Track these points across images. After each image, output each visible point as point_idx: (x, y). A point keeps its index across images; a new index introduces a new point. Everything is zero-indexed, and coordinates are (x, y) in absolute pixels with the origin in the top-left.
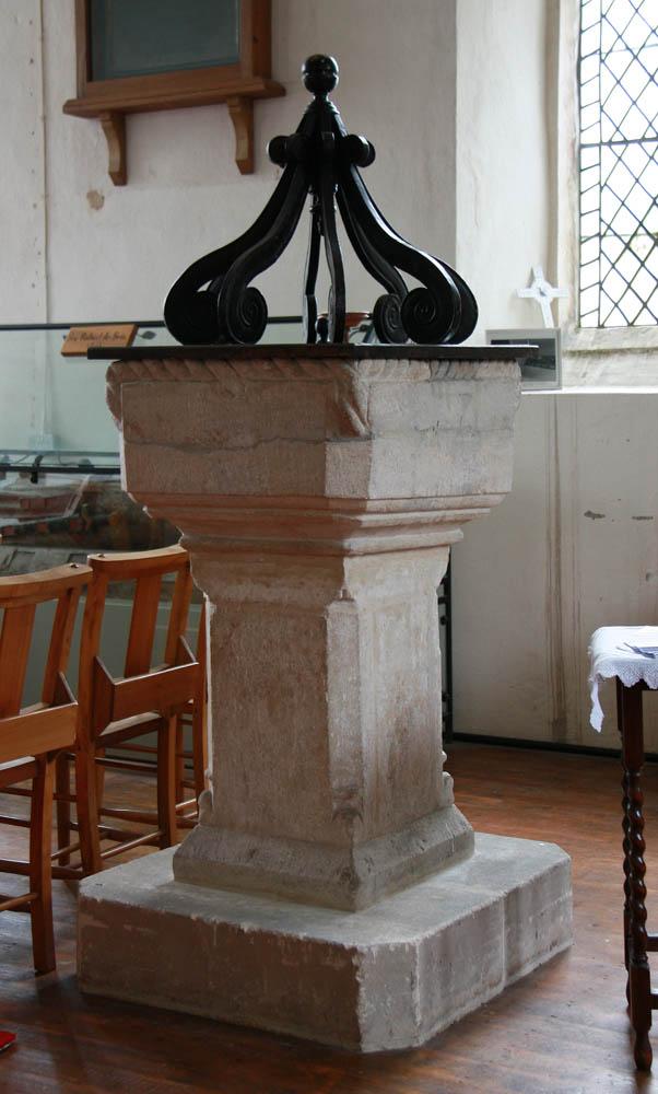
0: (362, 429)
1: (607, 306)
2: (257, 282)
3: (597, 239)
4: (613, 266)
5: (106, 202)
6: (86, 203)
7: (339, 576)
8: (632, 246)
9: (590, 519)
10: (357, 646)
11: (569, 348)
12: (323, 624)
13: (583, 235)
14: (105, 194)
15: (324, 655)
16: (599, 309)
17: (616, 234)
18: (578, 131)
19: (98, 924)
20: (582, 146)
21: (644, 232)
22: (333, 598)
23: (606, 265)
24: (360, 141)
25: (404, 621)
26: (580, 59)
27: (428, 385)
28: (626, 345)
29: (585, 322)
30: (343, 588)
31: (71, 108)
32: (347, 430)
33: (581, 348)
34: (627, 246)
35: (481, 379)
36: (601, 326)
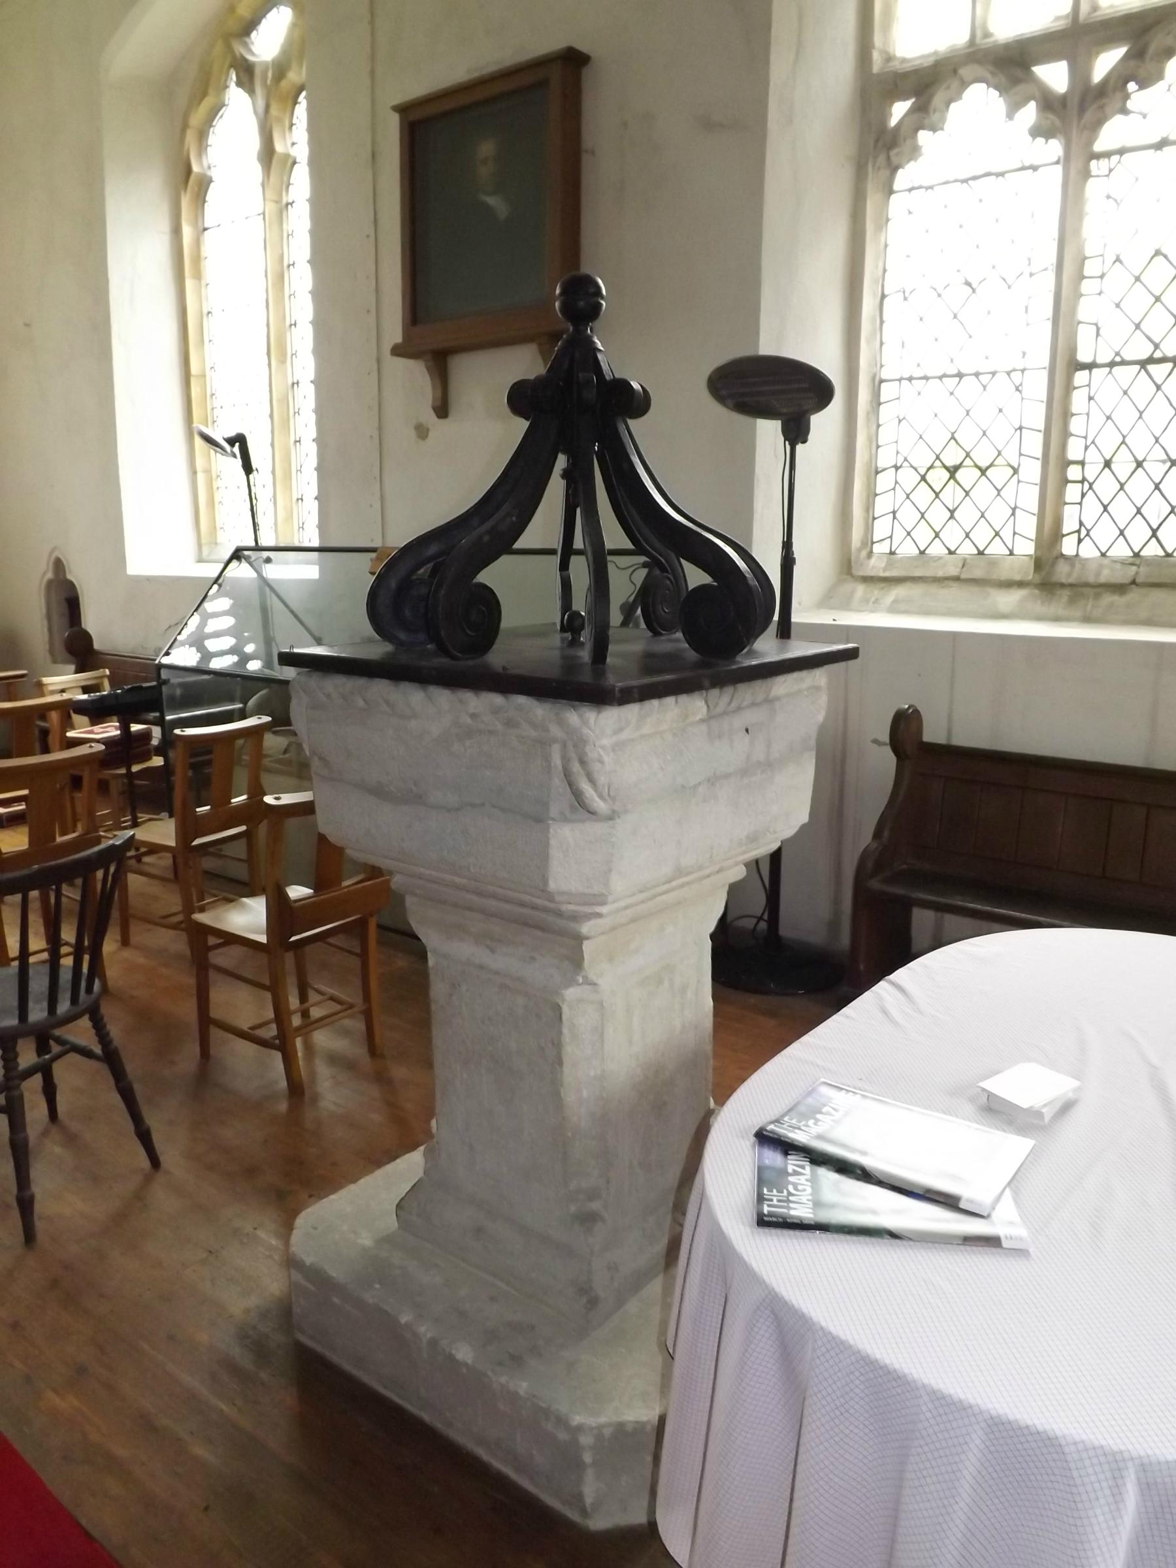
0: (600, 805)
1: (899, 534)
2: (484, 577)
3: (894, 469)
4: (908, 497)
5: (430, 434)
6: (412, 433)
7: (577, 961)
8: (928, 477)
9: (876, 746)
10: (602, 1036)
11: (861, 573)
12: (558, 1009)
13: (878, 465)
14: (430, 427)
15: (558, 1045)
16: (891, 537)
17: (916, 469)
18: (879, 365)
19: (303, 1282)
20: (882, 381)
21: (940, 465)
22: (572, 982)
23: (901, 496)
24: (68, 635)
25: (666, 984)
26: (883, 296)
27: (704, 727)
28: (918, 573)
29: (877, 549)
30: (584, 973)
31: (397, 351)
32: (580, 805)
33: (872, 574)
34: (923, 478)
35: (778, 699)
36: (892, 553)
